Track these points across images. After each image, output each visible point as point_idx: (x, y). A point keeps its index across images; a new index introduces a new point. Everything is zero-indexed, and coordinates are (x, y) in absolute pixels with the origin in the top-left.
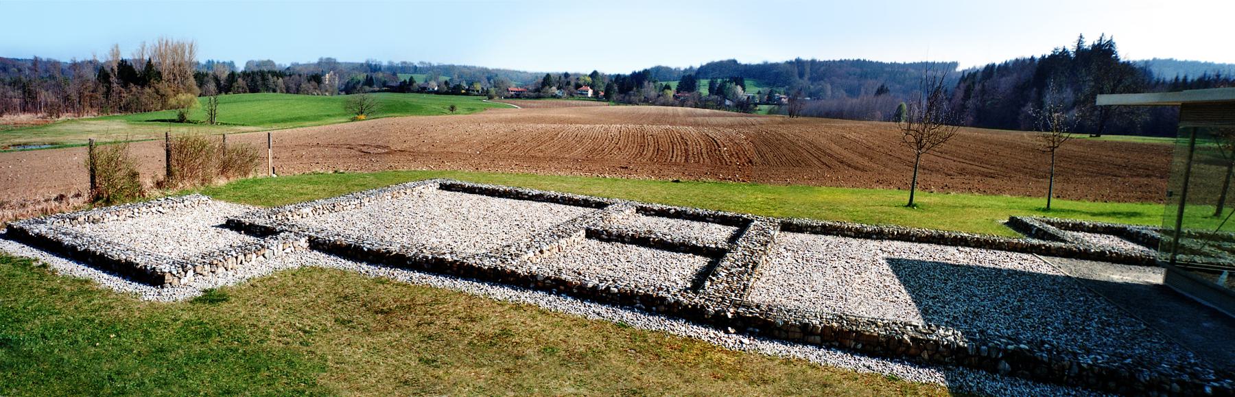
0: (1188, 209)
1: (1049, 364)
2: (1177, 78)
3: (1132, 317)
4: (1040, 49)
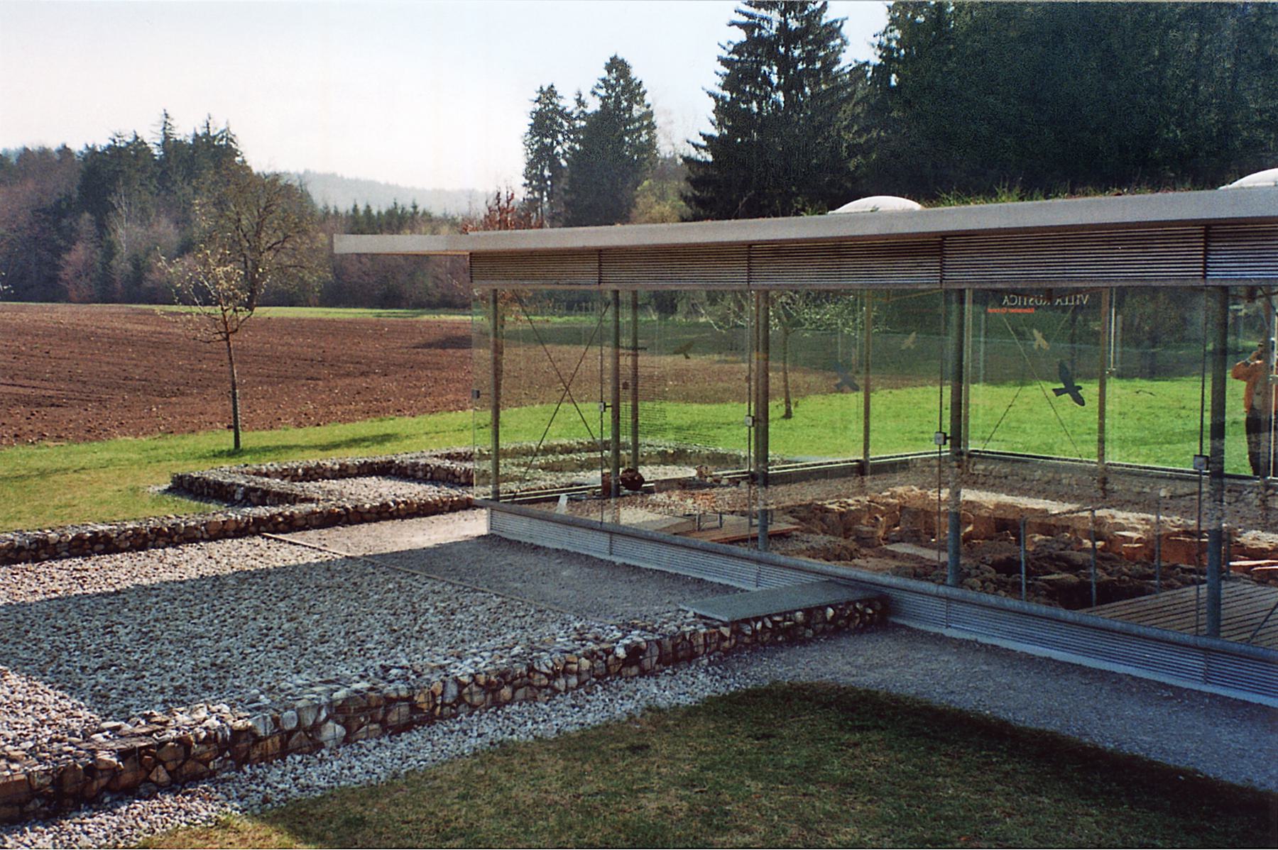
0: (874, 398)
1: (409, 699)
2: (355, 209)
3: (475, 591)
4: (84, 129)
